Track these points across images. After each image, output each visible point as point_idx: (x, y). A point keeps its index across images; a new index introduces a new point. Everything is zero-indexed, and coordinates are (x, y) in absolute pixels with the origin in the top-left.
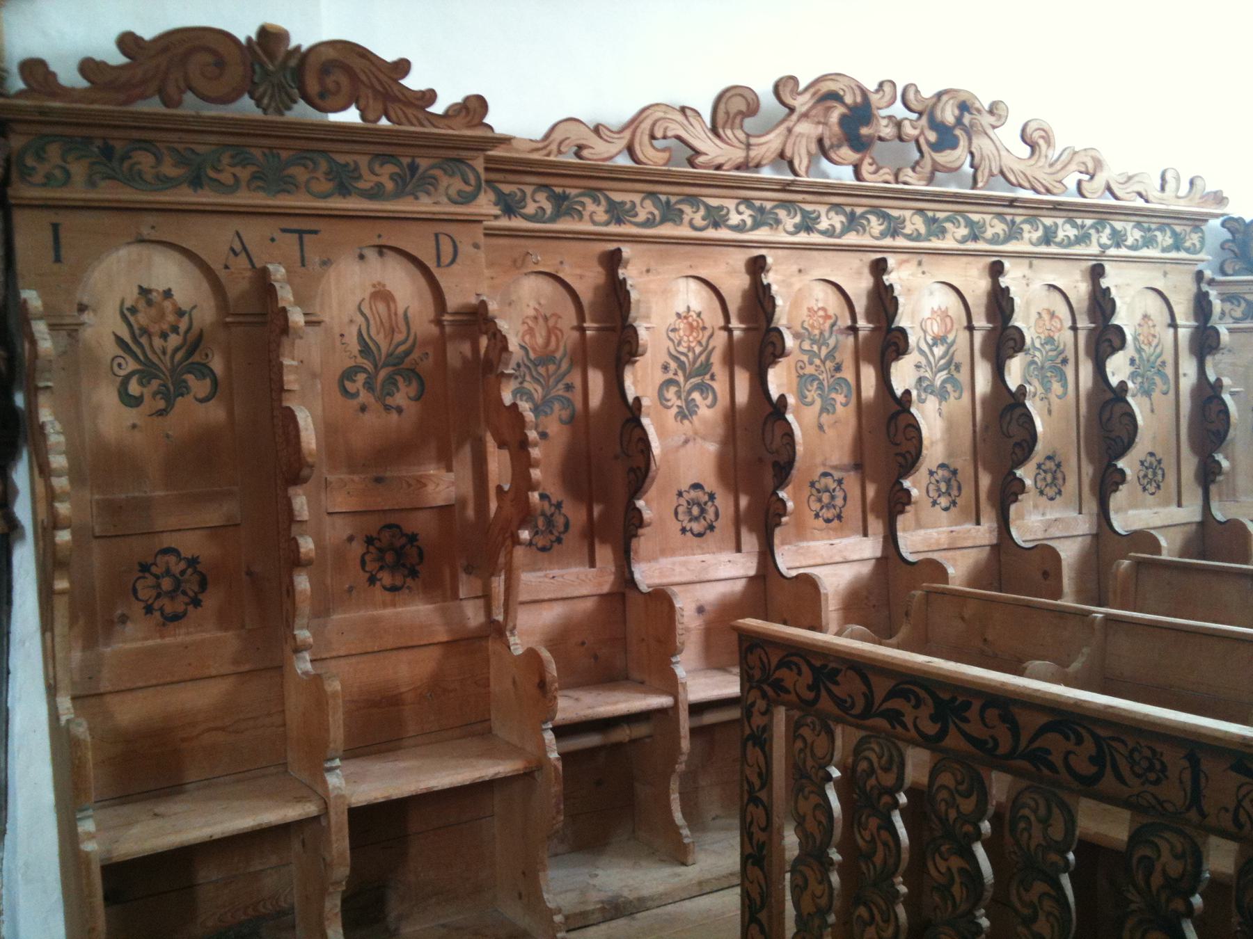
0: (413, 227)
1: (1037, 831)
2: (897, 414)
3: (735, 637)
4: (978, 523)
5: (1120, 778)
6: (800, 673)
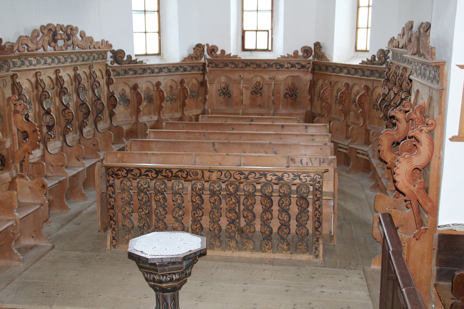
1: (177, 187)
3: (104, 168)
5: (191, 176)
6: (123, 171)
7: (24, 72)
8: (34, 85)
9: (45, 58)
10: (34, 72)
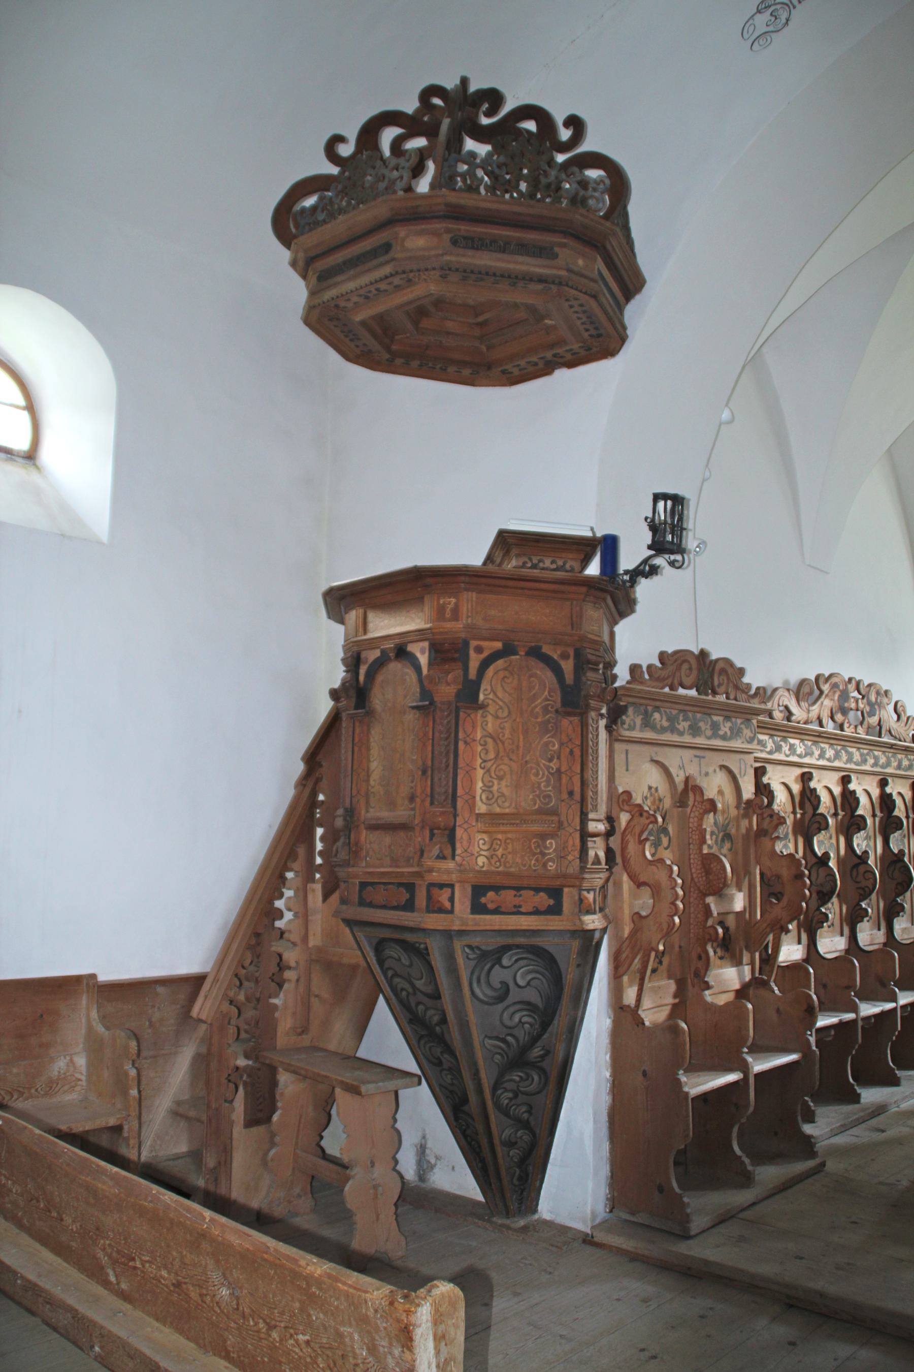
0: (733, 755)
2: (858, 864)
4: (879, 929)
7: (780, 767)
8: (797, 800)
9: (823, 745)
10: (798, 771)
